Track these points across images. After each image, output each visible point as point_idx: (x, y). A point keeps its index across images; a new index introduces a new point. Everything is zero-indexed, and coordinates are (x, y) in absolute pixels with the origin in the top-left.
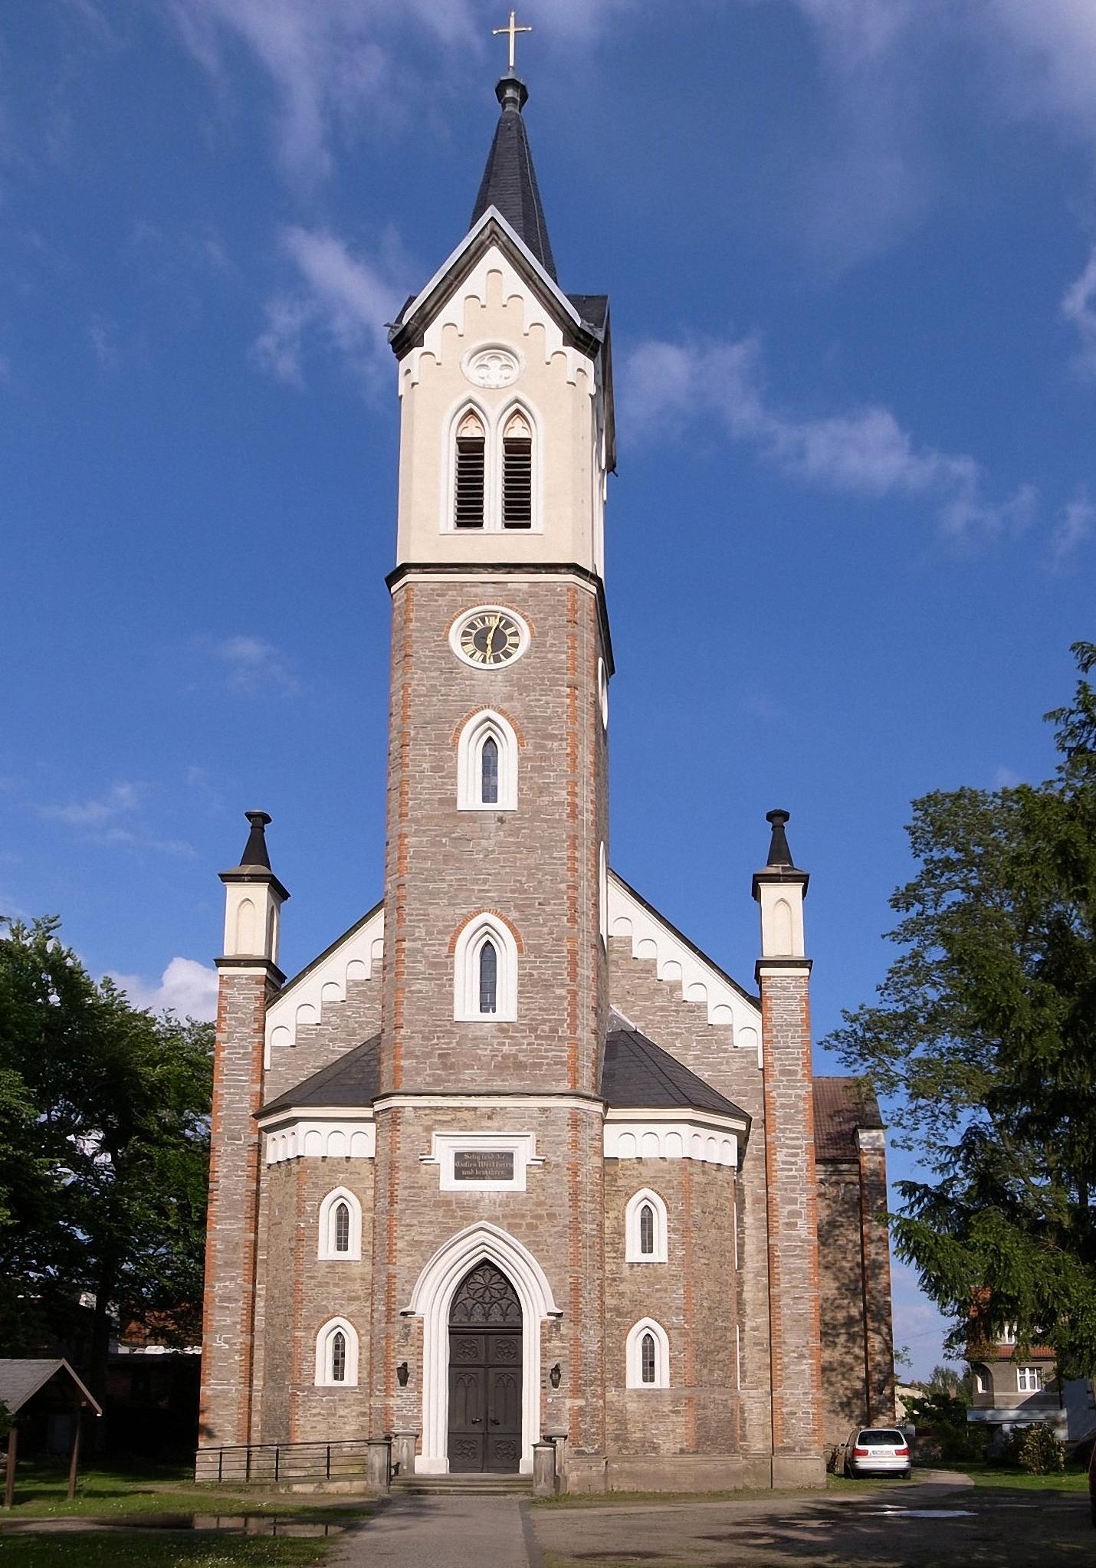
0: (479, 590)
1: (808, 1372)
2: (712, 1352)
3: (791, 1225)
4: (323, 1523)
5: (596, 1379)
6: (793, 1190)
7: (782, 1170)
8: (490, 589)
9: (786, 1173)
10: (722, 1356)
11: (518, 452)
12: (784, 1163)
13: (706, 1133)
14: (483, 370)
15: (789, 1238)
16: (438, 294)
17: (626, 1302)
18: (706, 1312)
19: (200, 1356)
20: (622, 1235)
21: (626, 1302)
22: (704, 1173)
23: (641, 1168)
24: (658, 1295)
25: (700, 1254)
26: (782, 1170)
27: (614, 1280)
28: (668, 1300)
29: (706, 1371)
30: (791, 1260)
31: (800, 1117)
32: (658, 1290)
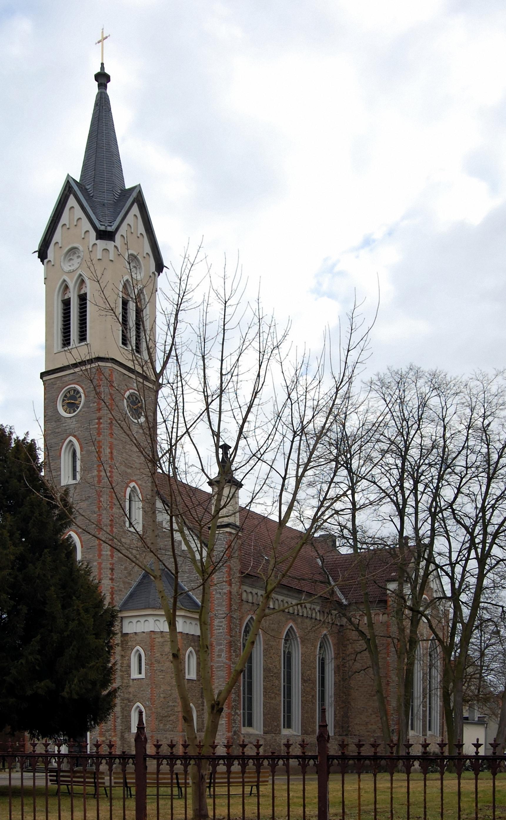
0: (66, 379)
1: (225, 724)
2: (166, 717)
3: (219, 656)
4: (145, 760)
5: (111, 729)
6: (221, 640)
7: (217, 629)
8: (71, 377)
9: (218, 631)
10: (172, 718)
11: (83, 298)
12: (218, 626)
13: (142, 620)
14: (71, 261)
15: (218, 662)
16: (50, 230)
17: (131, 696)
18: (162, 699)
19: (80, 705)
20: (130, 667)
21: (131, 696)
22: (162, 637)
23: (136, 637)
24: (142, 693)
25: (159, 674)
26: (217, 629)
27: (127, 686)
28: (145, 695)
29: (162, 725)
30: (219, 673)
31: (224, 603)
32: (142, 691)
